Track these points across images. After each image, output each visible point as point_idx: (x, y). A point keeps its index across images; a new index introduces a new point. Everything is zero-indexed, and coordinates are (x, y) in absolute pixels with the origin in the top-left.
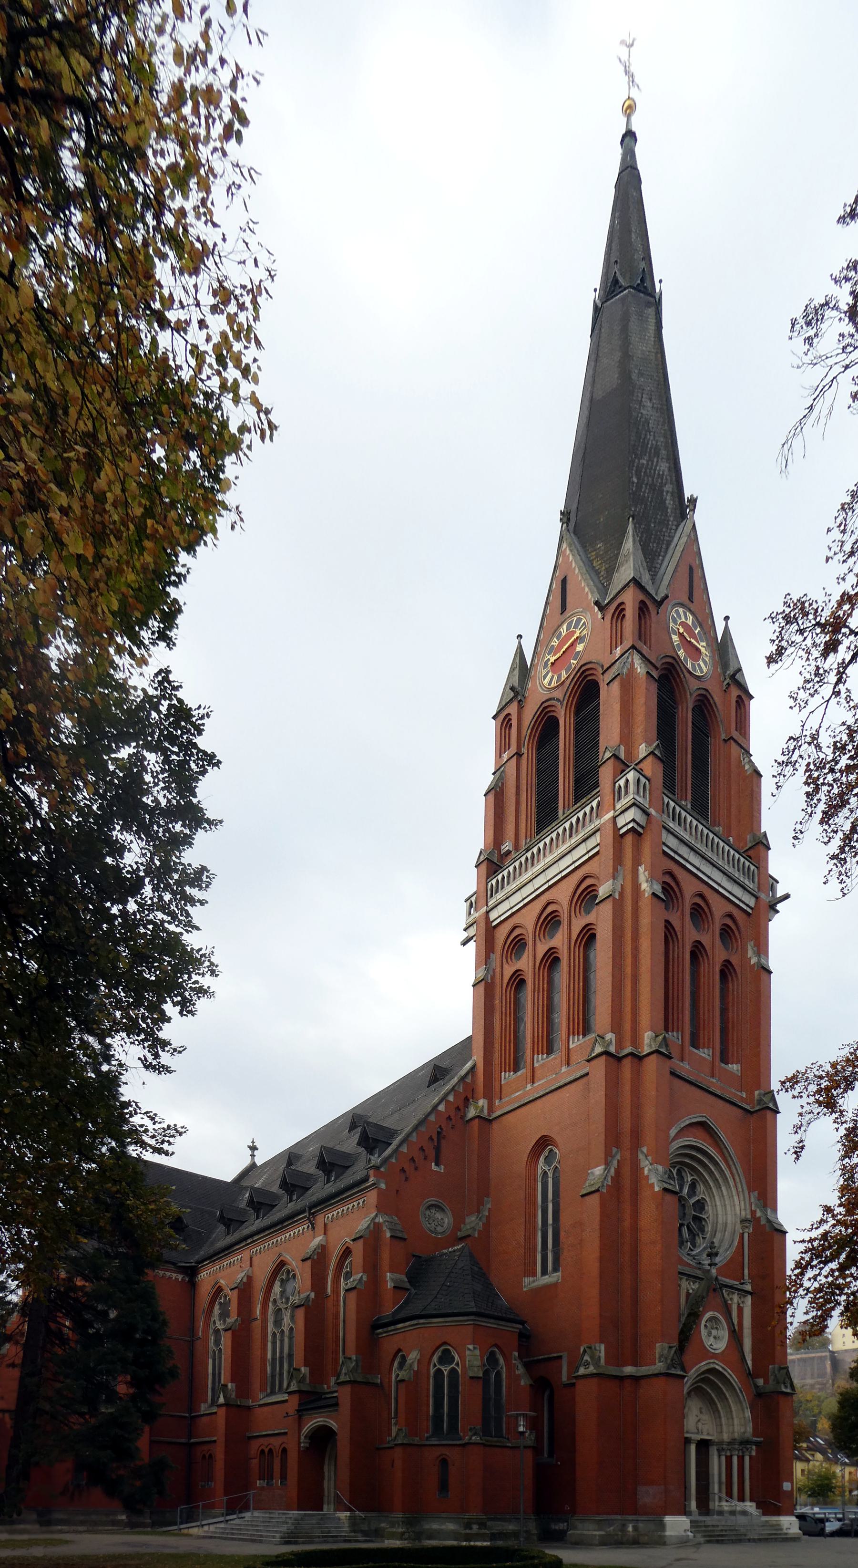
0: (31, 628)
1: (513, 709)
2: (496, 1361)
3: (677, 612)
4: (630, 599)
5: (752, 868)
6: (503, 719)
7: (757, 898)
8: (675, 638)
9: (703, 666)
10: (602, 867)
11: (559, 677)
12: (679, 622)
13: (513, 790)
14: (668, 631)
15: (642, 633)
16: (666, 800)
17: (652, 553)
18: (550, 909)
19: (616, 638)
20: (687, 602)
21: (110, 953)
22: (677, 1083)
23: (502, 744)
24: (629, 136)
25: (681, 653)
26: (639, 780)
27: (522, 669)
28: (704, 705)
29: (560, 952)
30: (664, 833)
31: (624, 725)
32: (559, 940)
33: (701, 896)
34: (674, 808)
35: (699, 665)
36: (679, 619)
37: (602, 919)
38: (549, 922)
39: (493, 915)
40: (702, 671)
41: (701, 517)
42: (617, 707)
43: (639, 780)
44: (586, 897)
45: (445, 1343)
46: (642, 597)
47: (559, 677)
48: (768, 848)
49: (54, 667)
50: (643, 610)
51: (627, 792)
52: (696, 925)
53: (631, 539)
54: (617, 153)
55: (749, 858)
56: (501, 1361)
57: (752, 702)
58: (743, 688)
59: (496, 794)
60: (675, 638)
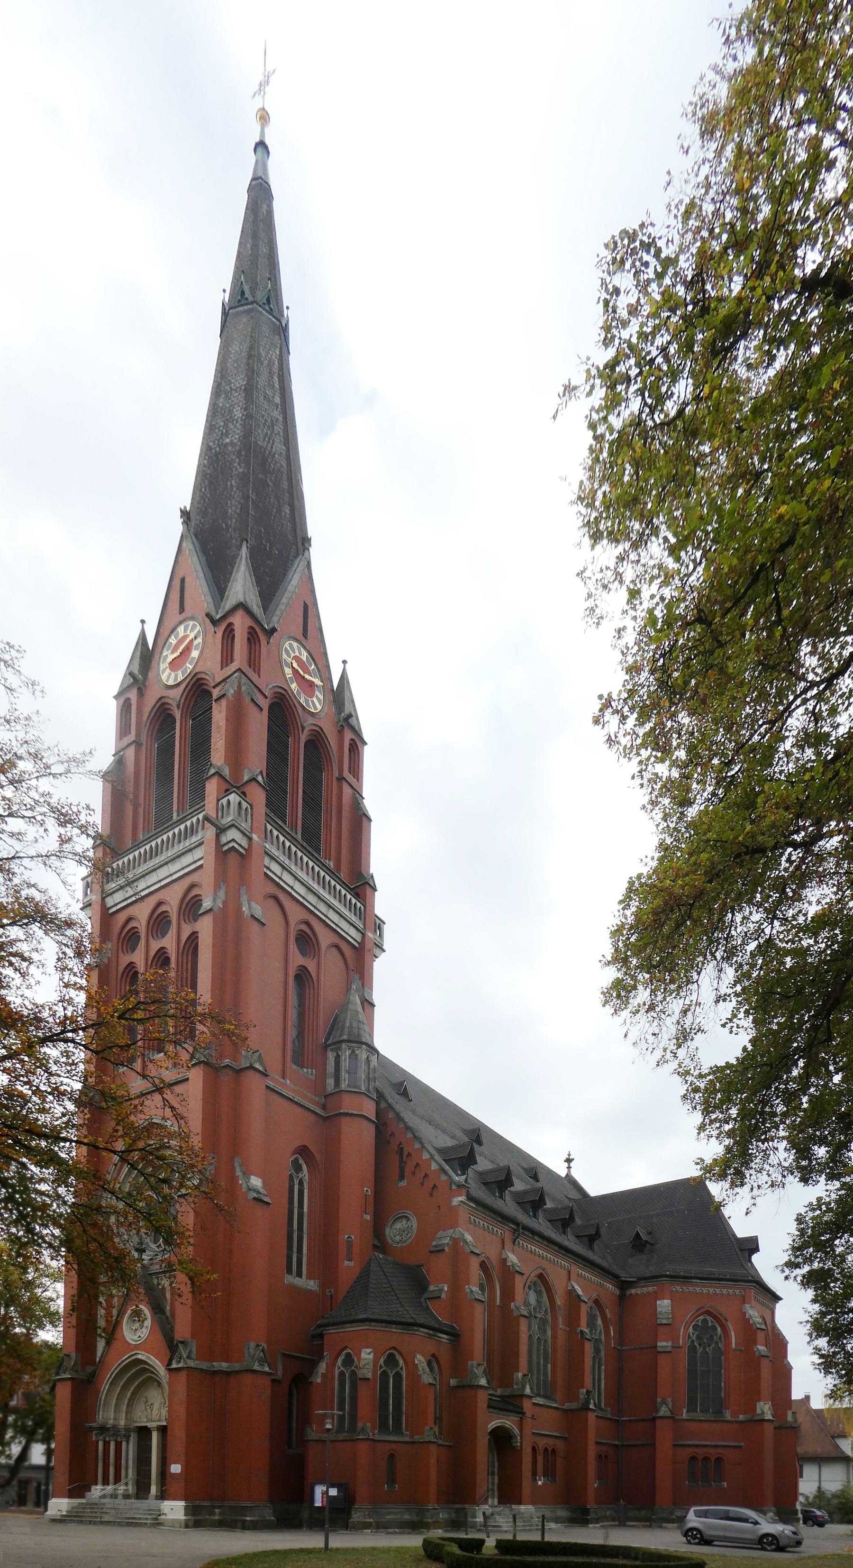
1: (133, 695)
2: (396, 1364)
3: (291, 646)
4: (240, 622)
5: (359, 905)
6: (125, 709)
7: (363, 935)
8: (288, 671)
9: (316, 703)
11: (176, 676)
12: (293, 655)
14: (280, 663)
16: (269, 827)
19: (227, 658)
20: (300, 637)
22: (270, 1093)
23: (123, 729)
25: (294, 686)
26: (240, 803)
27: (145, 656)
28: (316, 742)
29: (169, 951)
30: (267, 861)
31: (237, 741)
32: (169, 942)
33: (307, 923)
34: (277, 837)
35: (313, 702)
36: (292, 652)
37: (205, 927)
38: (159, 922)
39: (110, 902)
40: (315, 708)
41: (316, 553)
43: (240, 803)
44: (191, 907)
45: (394, 1348)
47: (176, 676)
48: (374, 889)
50: (252, 638)
51: (228, 813)
55: (357, 896)
56: (401, 1362)
57: (366, 748)
58: (357, 733)
60: (288, 671)
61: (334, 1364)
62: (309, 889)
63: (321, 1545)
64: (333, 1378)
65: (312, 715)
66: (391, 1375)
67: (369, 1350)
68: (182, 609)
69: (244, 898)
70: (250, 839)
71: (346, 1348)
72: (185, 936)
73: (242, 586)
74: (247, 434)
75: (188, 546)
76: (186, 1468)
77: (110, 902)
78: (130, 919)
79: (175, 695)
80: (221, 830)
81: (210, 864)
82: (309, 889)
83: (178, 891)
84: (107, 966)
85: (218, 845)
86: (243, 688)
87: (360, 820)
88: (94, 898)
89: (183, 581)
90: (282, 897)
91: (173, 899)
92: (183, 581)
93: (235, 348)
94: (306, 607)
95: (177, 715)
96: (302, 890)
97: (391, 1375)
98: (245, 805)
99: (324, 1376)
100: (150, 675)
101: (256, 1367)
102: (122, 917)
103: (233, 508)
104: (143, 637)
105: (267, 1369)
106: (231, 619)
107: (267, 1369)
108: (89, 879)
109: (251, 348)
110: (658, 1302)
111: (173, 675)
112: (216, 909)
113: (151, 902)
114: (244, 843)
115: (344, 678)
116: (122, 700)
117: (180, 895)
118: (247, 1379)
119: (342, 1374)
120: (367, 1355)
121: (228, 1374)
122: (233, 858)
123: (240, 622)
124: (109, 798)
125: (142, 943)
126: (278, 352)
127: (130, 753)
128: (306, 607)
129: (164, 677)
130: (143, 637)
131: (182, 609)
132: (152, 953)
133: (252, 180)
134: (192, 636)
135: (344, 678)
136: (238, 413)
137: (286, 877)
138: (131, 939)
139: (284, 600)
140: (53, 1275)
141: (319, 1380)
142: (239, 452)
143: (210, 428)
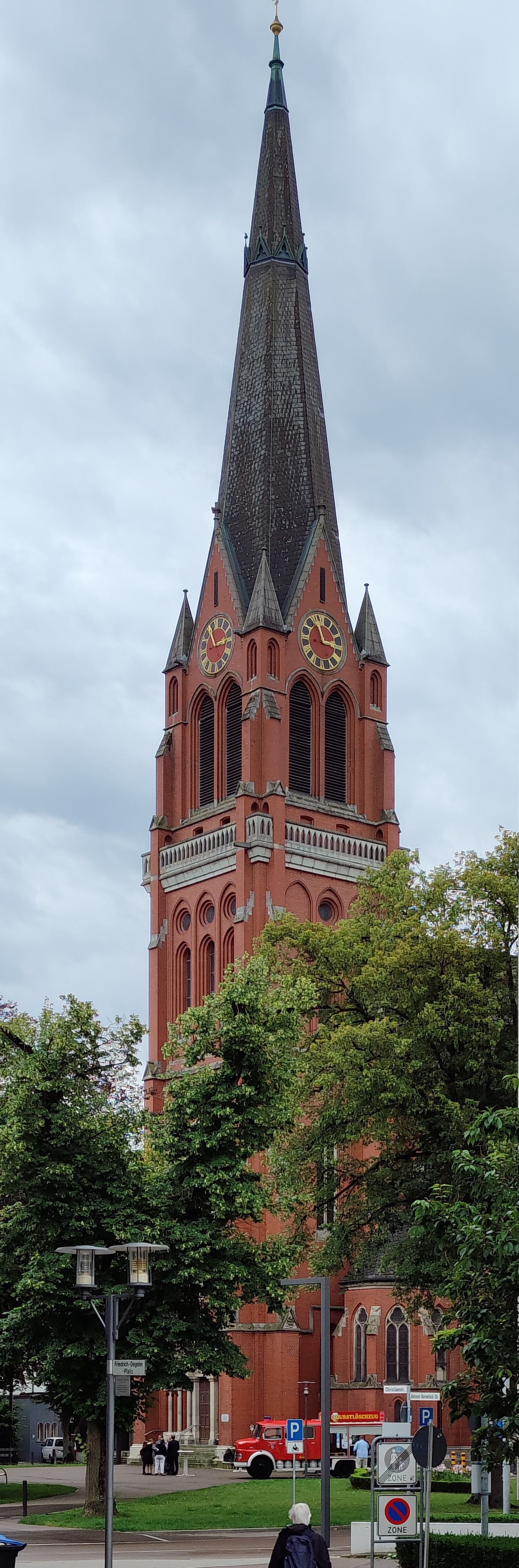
19: (252, 670)
24: (277, 63)
32: (212, 929)
33: (330, 890)
54: (267, 74)
61: (352, 1319)
64: (352, 1331)
66: (397, 1329)
67: (377, 1307)
68: (216, 603)
69: (269, 903)
71: (360, 1304)
74: (268, 411)
76: (233, 1415)
77: (165, 884)
81: (241, 872)
84: (165, 943)
86: (264, 705)
87: (383, 753)
88: (152, 879)
89: (216, 574)
90: (303, 879)
92: (216, 574)
93: (255, 311)
96: (322, 866)
97: (397, 1329)
99: (344, 1329)
101: (286, 1327)
102: (176, 898)
103: (257, 493)
105: (295, 1327)
107: (295, 1327)
108: (148, 857)
109: (269, 310)
112: (246, 920)
113: (199, 889)
114: (268, 854)
115: (366, 606)
116: (171, 675)
117: (198, 896)
118: (278, 1337)
119: (358, 1327)
120: (374, 1312)
121: (265, 1333)
122: (258, 870)
125: (192, 927)
126: (294, 299)
127: (178, 732)
131: (216, 603)
132: (200, 938)
133: (267, 107)
135: (366, 606)
136: (259, 387)
137: (308, 862)
139: (301, 585)
141: (340, 1334)
142: (261, 431)
143: (235, 403)
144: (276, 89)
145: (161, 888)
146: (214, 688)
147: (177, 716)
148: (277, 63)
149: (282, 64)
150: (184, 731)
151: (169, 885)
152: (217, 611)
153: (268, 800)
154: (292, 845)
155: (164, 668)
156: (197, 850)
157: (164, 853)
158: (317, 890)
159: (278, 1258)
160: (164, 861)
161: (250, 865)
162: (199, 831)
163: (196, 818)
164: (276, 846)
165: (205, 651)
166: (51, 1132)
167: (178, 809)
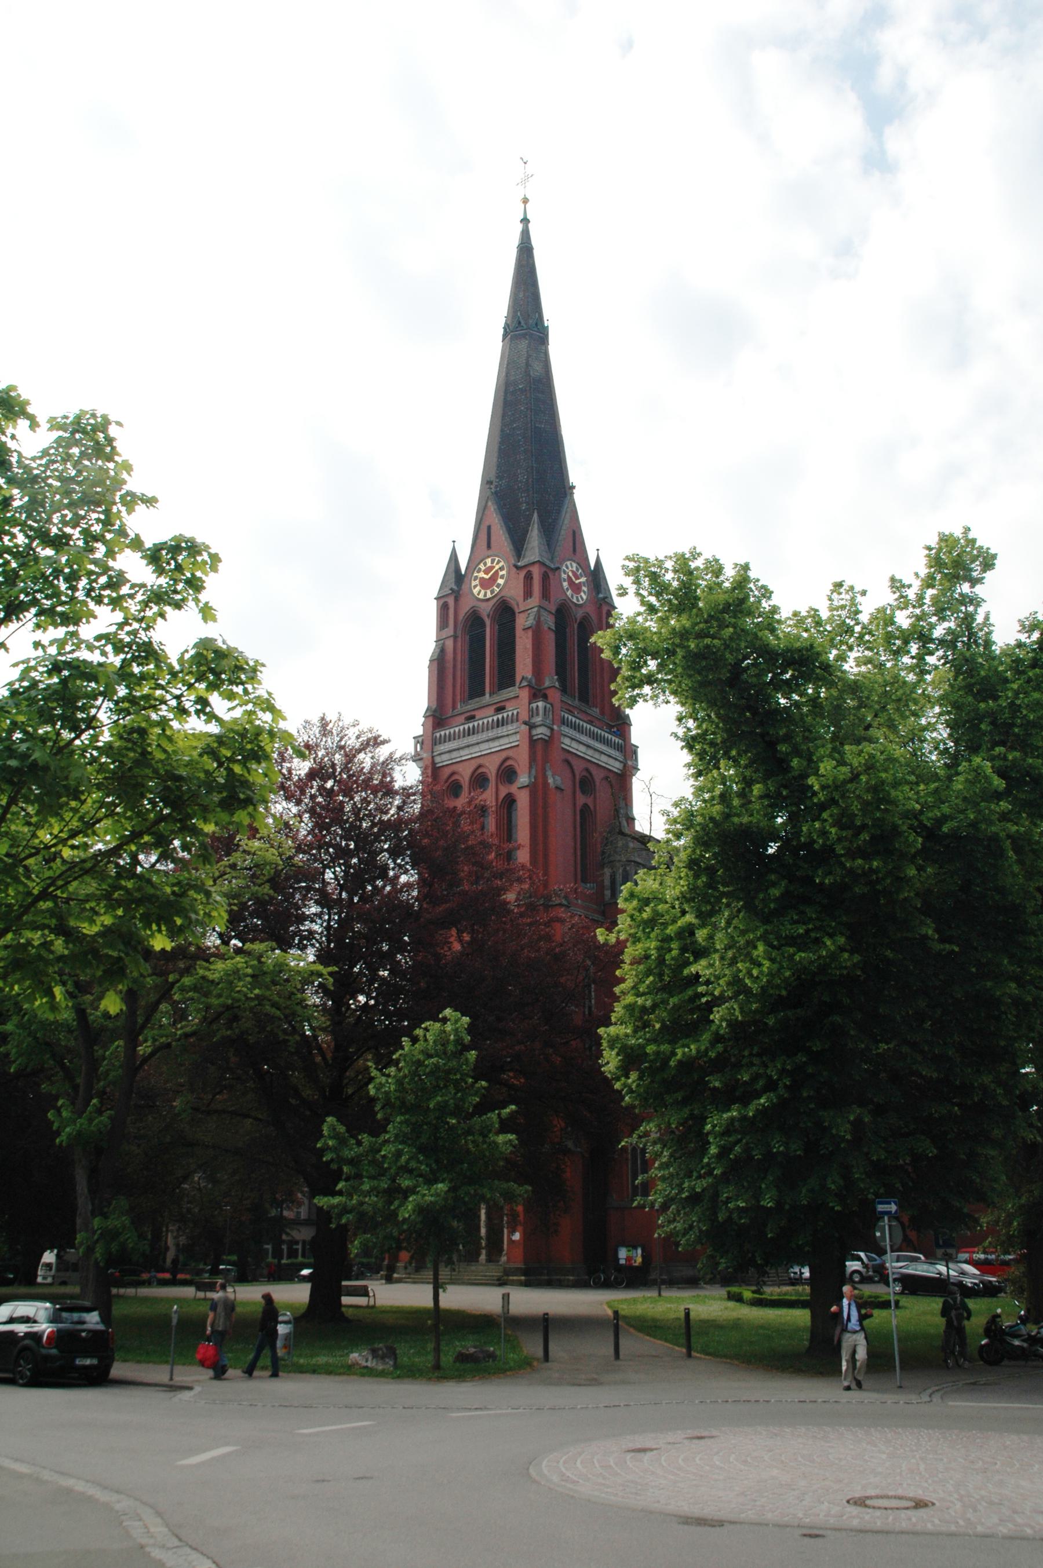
0: (26, 695)
1: (451, 601)
4: (536, 572)
6: (443, 610)
10: (522, 761)
13: (451, 670)
15: (545, 594)
17: (549, 531)
18: (480, 770)
19: (528, 594)
21: (67, 580)
24: (525, 221)
33: (587, 770)
38: (479, 780)
41: (578, 496)
42: (529, 661)
44: (507, 774)
46: (544, 569)
49: (57, 1141)
52: (583, 792)
53: (536, 526)
54: (520, 227)
59: (440, 664)
62: (588, 746)
63: (429, 1303)
65: (581, 606)
68: (489, 546)
69: (549, 773)
70: (552, 730)
72: (502, 795)
73: (534, 547)
75: (492, 507)
77: (437, 759)
78: (453, 774)
79: (485, 610)
80: (532, 727)
82: (588, 746)
83: (497, 760)
85: (531, 736)
89: (489, 528)
90: (570, 758)
91: (491, 768)
92: (489, 528)
94: (574, 532)
95: (488, 622)
96: (583, 748)
98: (548, 706)
100: (463, 587)
102: (447, 772)
104: (454, 557)
106: (531, 569)
110: (847, 1263)
111: (483, 592)
113: (473, 764)
115: (598, 562)
116: (442, 601)
117: (498, 763)
123: (536, 572)
124: (435, 679)
127: (450, 643)
128: (574, 532)
129: (475, 591)
130: (454, 557)
131: (489, 546)
134: (497, 567)
135: (598, 562)
138: (455, 789)
140: (184, 957)
144: (525, 235)
145: (433, 763)
146: (485, 610)
147: (450, 631)
148: (525, 221)
149: (529, 221)
150: (455, 642)
151: (442, 760)
152: (490, 552)
153: (548, 692)
154: (565, 729)
155: (435, 595)
156: (470, 732)
157: (438, 735)
158: (578, 766)
159: (404, 1088)
160: (435, 742)
161: (533, 742)
162: (471, 718)
163: (469, 707)
164: (555, 727)
165: (477, 582)
166: (433, 962)
167: (449, 701)
